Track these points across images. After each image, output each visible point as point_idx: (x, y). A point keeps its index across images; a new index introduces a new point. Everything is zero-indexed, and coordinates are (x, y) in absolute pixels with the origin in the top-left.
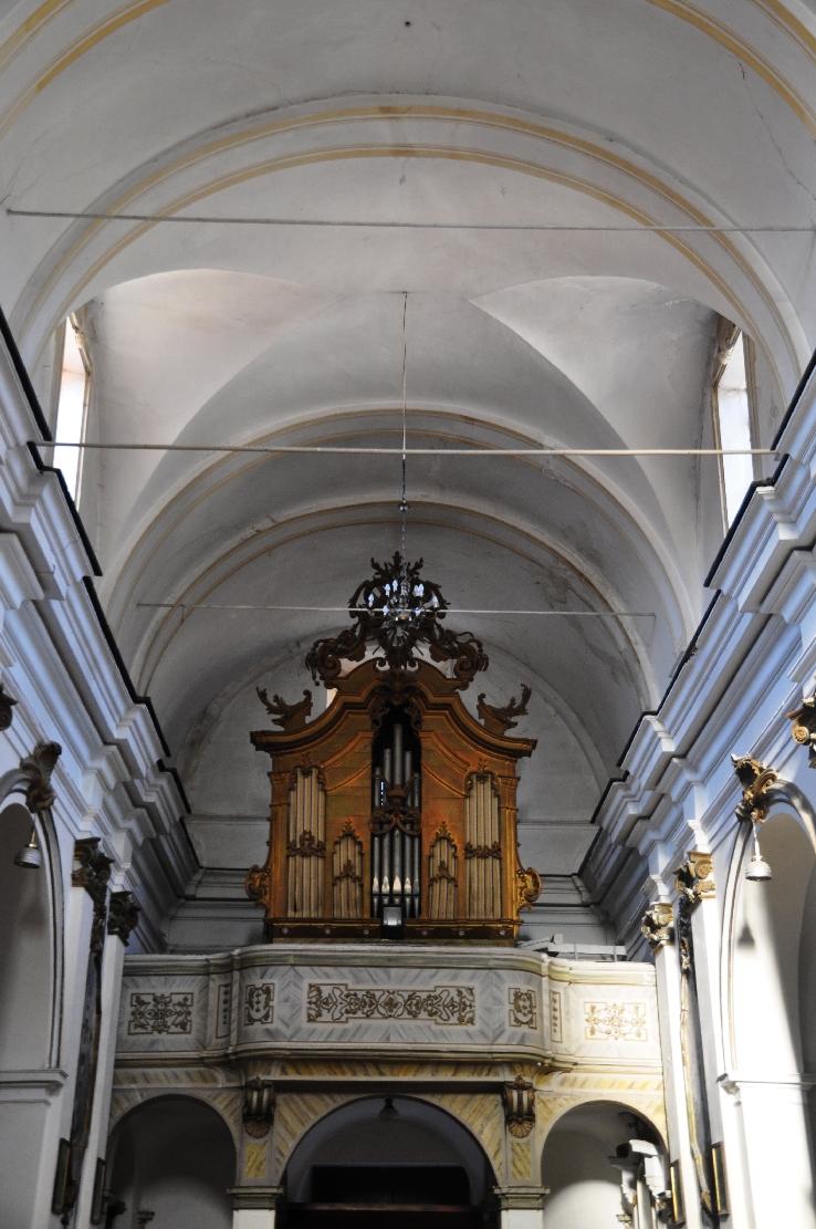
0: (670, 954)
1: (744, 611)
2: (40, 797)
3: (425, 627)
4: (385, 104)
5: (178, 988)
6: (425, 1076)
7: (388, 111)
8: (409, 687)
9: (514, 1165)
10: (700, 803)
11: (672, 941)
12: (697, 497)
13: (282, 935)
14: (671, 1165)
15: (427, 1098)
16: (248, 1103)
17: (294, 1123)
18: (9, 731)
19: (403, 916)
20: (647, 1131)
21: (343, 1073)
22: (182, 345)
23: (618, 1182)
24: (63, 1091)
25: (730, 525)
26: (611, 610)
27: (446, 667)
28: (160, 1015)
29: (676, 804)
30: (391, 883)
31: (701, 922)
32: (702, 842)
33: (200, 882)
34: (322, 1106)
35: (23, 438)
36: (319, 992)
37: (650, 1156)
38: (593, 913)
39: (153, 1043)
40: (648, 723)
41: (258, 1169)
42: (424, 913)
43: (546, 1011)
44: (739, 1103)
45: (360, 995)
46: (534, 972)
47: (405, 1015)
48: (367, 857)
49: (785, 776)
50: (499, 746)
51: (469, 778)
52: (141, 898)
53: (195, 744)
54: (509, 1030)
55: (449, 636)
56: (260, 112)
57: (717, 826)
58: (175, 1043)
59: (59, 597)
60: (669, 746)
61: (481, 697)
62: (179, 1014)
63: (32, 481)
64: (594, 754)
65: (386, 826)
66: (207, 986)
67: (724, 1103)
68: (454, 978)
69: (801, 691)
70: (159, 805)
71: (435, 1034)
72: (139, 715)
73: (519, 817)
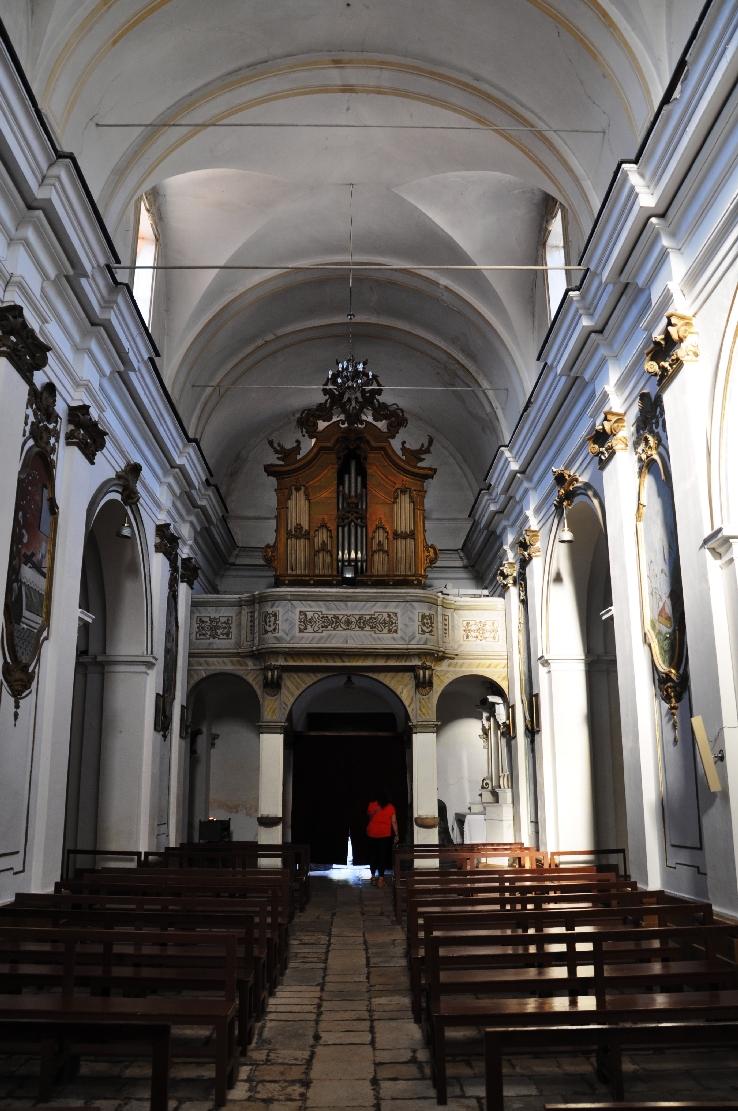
0: (513, 592)
1: (561, 375)
2: (130, 497)
3: (369, 400)
4: (335, 58)
5: (224, 613)
6: (369, 663)
7: (337, 63)
8: (360, 437)
9: (420, 709)
11: (515, 584)
12: (534, 316)
14: (510, 708)
15: (370, 675)
16: (266, 678)
17: (293, 689)
19: (356, 572)
20: (498, 690)
22: (210, 217)
23: (481, 718)
24: (155, 668)
25: (553, 317)
26: (480, 387)
27: (382, 425)
28: (214, 629)
29: (518, 503)
30: (349, 554)
31: (532, 572)
32: (533, 523)
33: (237, 555)
35: (102, 261)
38: (470, 572)
39: (210, 644)
40: (503, 452)
41: (274, 711)
42: (369, 570)
44: (549, 672)
48: (335, 538)
50: (415, 473)
52: (200, 560)
53: (233, 475)
55: (384, 406)
56: (256, 64)
57: (543, 513)
58: (222, 644)
59: (86, 275)
60: (514, 466)
62: (225, 628)
64: (470, 476)
66: (240, 613)
68: (386, 607)
69: (595, 425)
71: (374, 639)
72: (191, 450)
73: (426, 515)
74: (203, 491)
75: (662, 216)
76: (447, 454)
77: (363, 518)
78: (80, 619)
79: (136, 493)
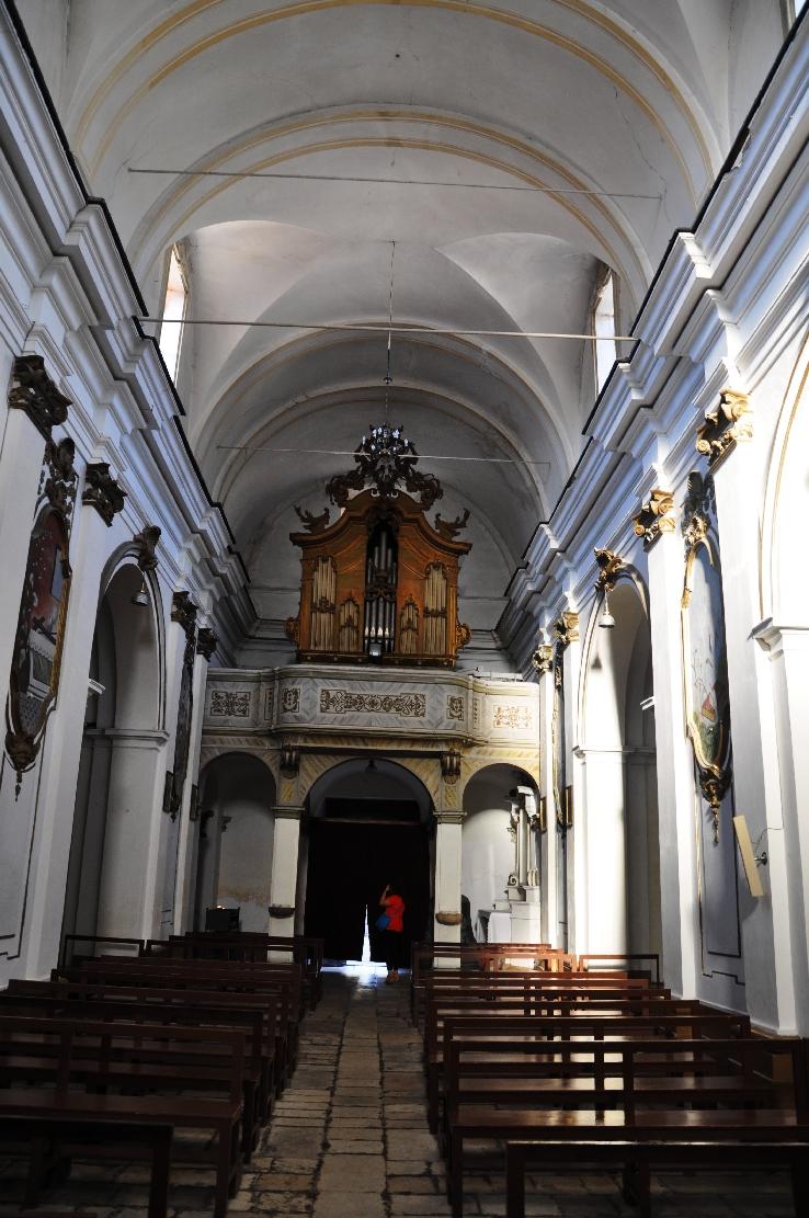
0: (549, 677)
1: (607, 451)
2: (148, 561)
3: (403, 468)
5: (241, 689)
6: (394, 747)
7: (384, 115)
8: (392, 508)
10: (573, 582)
11: (551, 668)
12: (580, 387)
13: (307, 661)
14: (541, 800)
15: (395, 760)
16: (283, 759)
17: (312, 773)
18: (123, 512)
19: (383, 650)
20: (528, 780)
21: (342, 744)
22: (245, 270)
23: (509, 810)
24: (167, 744)
27: (416, 496)
28: (230, 704)
31: (569, 656)
32: (573, 605)
34: (330, 762)
35: (129, 313)
36: (328, 693)
37: (529, 795)
38: (502, 654)
40: (682, 245)
43: (470, 710)
44: (584, 763)
45: (354, 697)
46: (464, 686)
47: (382, 710)
49: (627, 560)
50: (449, 548)
51: (428, 566)
52: (217, 631)
53: (257, 542)
54: (446, 721)
55: (419, 476)
59: (157, 428)
60: (554, 544)
61: (438, 515)
62: (242, 705)
63: (137, 345)
64: (508, 554)
65: (374, 596)
67: (576, 764)
68: (413, 689)
70: (210, 532)
72: (214, 514)
74: (224, 558)
75: (719, 288)
76: (483, 528)
77: (393, 593)
78: (90, 689)
79: (154, 558)
